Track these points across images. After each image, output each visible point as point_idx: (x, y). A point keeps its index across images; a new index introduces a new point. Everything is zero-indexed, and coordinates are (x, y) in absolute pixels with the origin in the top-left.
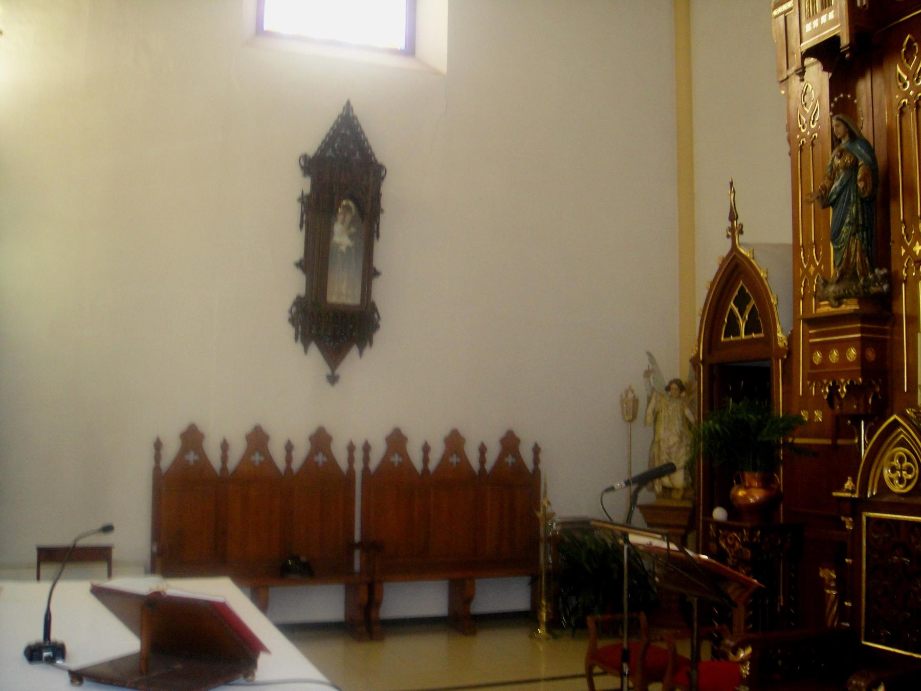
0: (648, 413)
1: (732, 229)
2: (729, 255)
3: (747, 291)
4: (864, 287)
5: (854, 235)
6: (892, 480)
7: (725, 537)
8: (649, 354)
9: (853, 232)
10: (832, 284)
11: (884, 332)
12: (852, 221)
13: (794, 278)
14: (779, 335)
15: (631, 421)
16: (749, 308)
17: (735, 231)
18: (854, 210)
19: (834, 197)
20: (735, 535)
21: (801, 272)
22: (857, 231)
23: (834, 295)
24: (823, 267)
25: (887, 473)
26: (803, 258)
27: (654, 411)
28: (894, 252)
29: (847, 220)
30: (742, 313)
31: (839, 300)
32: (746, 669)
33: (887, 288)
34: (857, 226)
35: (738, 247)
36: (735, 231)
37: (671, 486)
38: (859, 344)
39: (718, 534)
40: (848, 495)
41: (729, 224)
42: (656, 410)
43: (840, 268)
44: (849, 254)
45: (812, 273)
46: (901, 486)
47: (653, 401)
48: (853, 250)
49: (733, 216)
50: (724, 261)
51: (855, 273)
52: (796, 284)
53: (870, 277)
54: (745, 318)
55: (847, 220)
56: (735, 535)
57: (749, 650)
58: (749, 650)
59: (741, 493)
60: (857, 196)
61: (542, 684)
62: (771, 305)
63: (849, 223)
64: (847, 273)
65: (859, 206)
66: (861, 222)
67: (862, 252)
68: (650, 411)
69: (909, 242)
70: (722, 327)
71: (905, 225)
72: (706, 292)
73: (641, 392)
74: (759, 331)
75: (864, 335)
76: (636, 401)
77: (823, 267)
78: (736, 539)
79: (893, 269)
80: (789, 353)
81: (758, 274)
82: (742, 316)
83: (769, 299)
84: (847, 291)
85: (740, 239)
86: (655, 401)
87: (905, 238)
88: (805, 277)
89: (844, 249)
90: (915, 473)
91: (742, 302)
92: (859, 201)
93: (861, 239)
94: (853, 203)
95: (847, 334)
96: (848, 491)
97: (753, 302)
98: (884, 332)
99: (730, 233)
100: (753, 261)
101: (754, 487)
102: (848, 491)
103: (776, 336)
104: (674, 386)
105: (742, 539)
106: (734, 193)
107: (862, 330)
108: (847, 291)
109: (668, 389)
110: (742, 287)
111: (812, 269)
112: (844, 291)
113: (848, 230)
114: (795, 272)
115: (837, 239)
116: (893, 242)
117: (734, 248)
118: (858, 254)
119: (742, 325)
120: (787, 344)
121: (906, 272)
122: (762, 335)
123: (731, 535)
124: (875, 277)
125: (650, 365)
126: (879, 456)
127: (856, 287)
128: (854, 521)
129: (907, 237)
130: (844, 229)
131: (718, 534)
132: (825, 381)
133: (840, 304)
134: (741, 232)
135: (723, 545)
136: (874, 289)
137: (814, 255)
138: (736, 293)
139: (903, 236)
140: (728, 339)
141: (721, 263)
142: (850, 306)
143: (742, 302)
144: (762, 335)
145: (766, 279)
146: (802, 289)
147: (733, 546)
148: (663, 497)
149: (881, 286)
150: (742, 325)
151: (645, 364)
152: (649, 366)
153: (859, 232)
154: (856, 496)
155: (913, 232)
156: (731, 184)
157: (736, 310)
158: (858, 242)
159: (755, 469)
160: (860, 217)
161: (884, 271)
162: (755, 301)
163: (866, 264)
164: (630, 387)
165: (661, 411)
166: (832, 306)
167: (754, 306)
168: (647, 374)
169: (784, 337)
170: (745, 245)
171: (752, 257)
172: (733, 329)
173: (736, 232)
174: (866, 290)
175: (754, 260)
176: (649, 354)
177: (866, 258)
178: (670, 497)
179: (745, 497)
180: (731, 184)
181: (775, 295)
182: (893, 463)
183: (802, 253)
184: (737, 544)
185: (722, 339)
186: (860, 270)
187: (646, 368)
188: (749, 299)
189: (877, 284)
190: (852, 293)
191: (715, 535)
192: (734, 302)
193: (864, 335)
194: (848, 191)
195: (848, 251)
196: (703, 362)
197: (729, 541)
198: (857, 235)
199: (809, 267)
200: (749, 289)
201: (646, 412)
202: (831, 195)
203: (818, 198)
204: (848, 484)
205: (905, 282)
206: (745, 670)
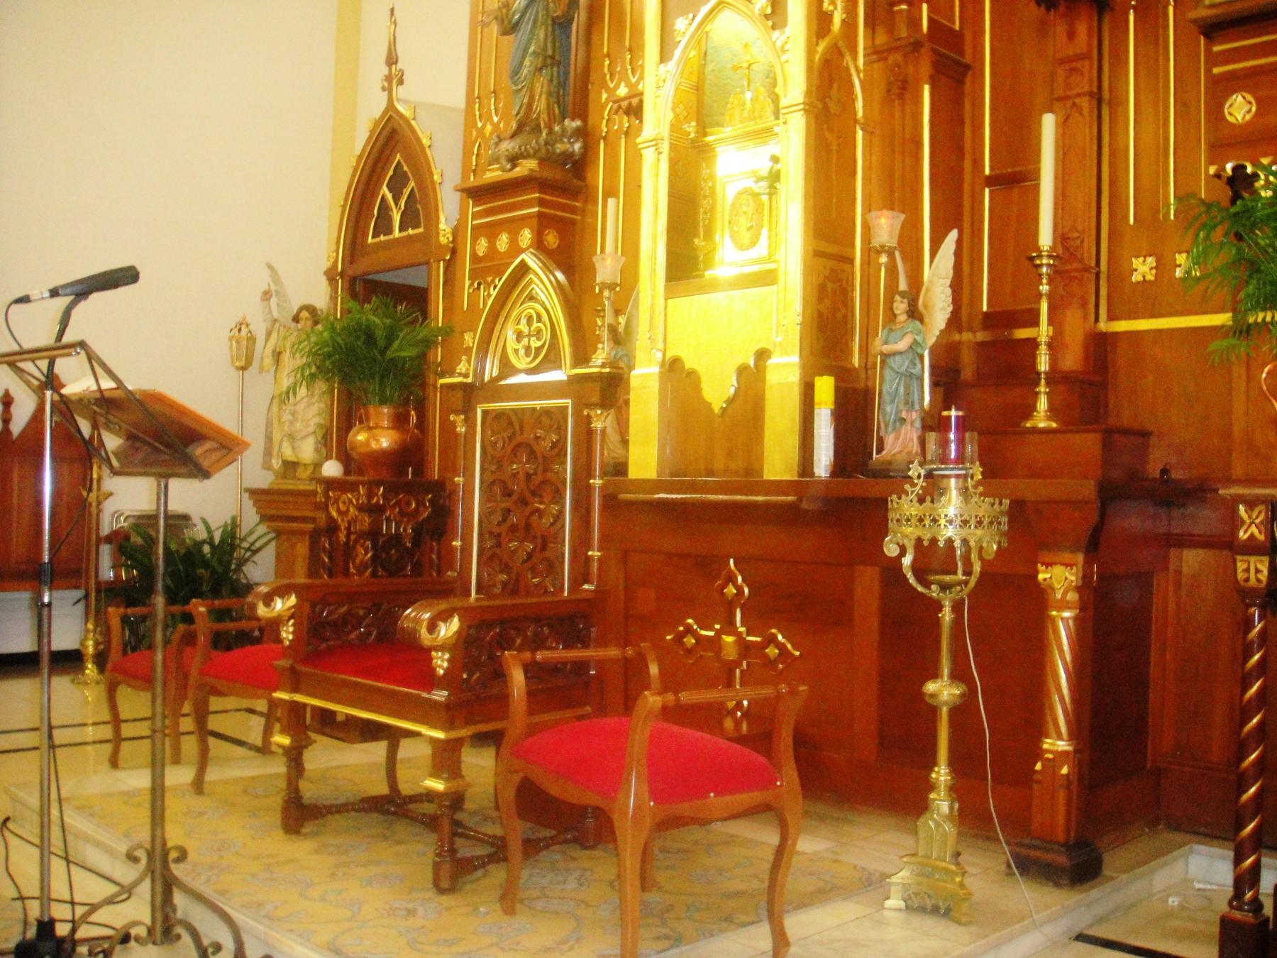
0: (265, 354)
1: (389, 78)
2: (382, 116)
3: (405, 168)
4: (547, 143)
5: (540, 69)
6: (516, 351)
7: (337, 501)
8: (270, 267)
9: (539, 66)
10: (505, 139)
11: (573, 210)
12: (538, 51)
13: (465, 142)
14: (442, 226)
15: (243, 368)
16: (406, 192)
17: (393, 80)
18: (542, 36)
19: (517, 17)
20: (350, 496)
21: (474, 133)
22: (544, 66)
23: (507, 153)
24: (501, 125)
25: (511, 343)
26: (477, 113)
27: (274, 351)
28: (592, 97)
29: (532, 49)
30: (396, 199)
31: (514, 160)
32: (287, 632)
33: (580, 148)
34: (545, 58)
35: (396, 103)
36: (393, 80)
37: (296, 460)
38: (535, 222)
39: (328, 497)
40: (460, 379)
41: (385, 71)
42: (278, 350)
43: (519, 117)
44: (532, 98)
45: (488, 134)
46: (529, 359)
47: (274, 336)
48: (539, 90)
49: (392, 60)
50: (377, 123)
51: (539, 125)
52: (467, 153)
53: (557, 128)
54: (400, 208)
55: (532, 49)
56: (350, 496)
57: (293, 600)
58: (293, 600)
59: (361, 437)
60: (547, 15)
61: (89, 748)
62: (433, 182)
63: (534, 52)
64: (525, 126)
65: (550, 29)
66: (550, 52)
67: (550, 94)
68: (269, 351)
69: (612, 82)
70: (371, 223)
71: (609, 59)
72: (350, 171)
73: (259, 329)
74: (416, 226)
75: (543, 210)
76: (252, 339)
77: (501, 125)
78: (350, 501)
79: (590, 122)
80: (454, 252)
81: (419, 140)
82: (396, 204)
83: (432, 174)
84: (523, 148)
85: (400, 92)
86: (276, 336)
87: (608, 76)
88: (479, 140)
89: (525, 89)
90: (545, 341)
91: (397, 185)
92: (550, 22)
93: (549, 78)
94: (542, 24)
95: (521, 209)
96: (460, 374)
97: (412, 184)
98: (573, 210)
99: (386, 84)
100: (413, 122)
101: (382, 428)
102: (460, 374)
103: (437, 227)
104: (305, 314)
105: (357, 500)
106: (396, 25)
107: (541, 202)
108: (523, 148)
109: (296, 319)
110: (399, 163)
111: (489, 127)
112: (520, 147)
113: (531, 63)
114: (467, 133)
115: (516, 78)
116: (593, 84)
117: (390, 105)
118: (544, 96)
119: (397, 218)
120: (451, 239)
121: (607, 126)
122: (421, 230)
123: (344, 497)
124: (564, 130)
125: (271, 284)
126: (501, 320)
127: (536, 142)
128: (466, 420)
129: (611, 76)
130: (527, 62)
131: (328, 497)
132: (489, 279)
133: (514, 166)
134: (401, 82)
135: (334, 514)
136: (559, 148)
137: (493, 107)
138: (391, 173)
139: (605, 75)
140: (377, 240)
141: (372, 128)
142: (527, 166)
143: (397, 185)
144: (421, 230)
145: (429, 147)
146: (474, 157)
147: (346, 513)
148: (284, 477)
149: (572, 144)
150: (397, 218)
151: (264, 282)
152: (269, 284)
153: (547, 66)
154: (469, 380)
155: (618, 69)
156: (392, 11)
157: (389, 196)
158: (546, 82)
159: (383, 401)
160: (549, 46)
161: (577, 123)
162: (415, 182)
163: (554, 115)
164: (244, 318)
165: (285, 351)
166: (504, 170)
167: (412, 189)
168: (267, 295)
169: (449, 230)
170: (406, 102)
171: (412, 117)
172: (384, 225)
173: (394, 81)
174: (550, 148)
175: (416, 122)
176: (270, 267)
177: (556, 106)
178: (294, 478)
179: (367, 443)
180: (392, 11)
181: (440, 171)
182: (518, 327)
183: (477, 106)
184: (352, 510)
185: (370, 240)
186: (544, 120)
187: (265, 287)
188: (409, 180)
189: (566, 140)
190: (532, 152)
191: (323, 500)
192: (387, 185)
193: (543, 210)
194: (535, 9)
195: (531, 92)
196: (342, 274)
197: (341, 505)
198: (544, 71)
199: (484, 126)
200: (408, 166)
201: (263, 353)
202: (514, 12)
203: (496, 18)
204: (462, 367)
205: (605, 138)
206: (287, 634)
